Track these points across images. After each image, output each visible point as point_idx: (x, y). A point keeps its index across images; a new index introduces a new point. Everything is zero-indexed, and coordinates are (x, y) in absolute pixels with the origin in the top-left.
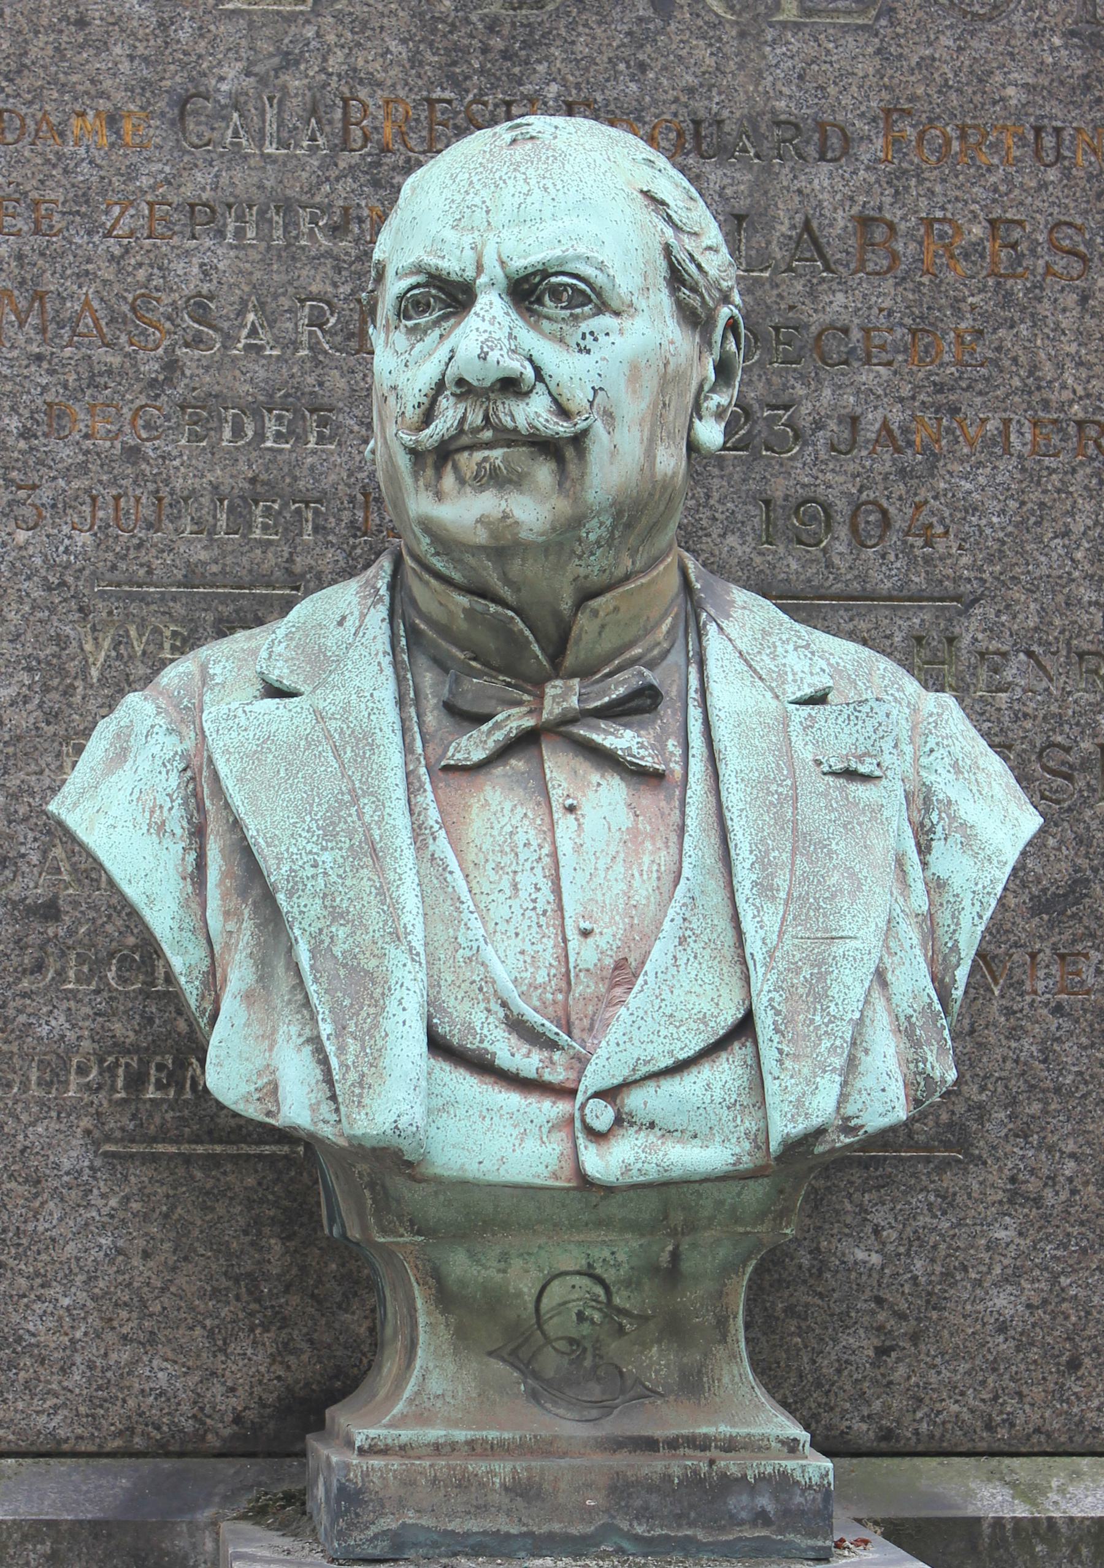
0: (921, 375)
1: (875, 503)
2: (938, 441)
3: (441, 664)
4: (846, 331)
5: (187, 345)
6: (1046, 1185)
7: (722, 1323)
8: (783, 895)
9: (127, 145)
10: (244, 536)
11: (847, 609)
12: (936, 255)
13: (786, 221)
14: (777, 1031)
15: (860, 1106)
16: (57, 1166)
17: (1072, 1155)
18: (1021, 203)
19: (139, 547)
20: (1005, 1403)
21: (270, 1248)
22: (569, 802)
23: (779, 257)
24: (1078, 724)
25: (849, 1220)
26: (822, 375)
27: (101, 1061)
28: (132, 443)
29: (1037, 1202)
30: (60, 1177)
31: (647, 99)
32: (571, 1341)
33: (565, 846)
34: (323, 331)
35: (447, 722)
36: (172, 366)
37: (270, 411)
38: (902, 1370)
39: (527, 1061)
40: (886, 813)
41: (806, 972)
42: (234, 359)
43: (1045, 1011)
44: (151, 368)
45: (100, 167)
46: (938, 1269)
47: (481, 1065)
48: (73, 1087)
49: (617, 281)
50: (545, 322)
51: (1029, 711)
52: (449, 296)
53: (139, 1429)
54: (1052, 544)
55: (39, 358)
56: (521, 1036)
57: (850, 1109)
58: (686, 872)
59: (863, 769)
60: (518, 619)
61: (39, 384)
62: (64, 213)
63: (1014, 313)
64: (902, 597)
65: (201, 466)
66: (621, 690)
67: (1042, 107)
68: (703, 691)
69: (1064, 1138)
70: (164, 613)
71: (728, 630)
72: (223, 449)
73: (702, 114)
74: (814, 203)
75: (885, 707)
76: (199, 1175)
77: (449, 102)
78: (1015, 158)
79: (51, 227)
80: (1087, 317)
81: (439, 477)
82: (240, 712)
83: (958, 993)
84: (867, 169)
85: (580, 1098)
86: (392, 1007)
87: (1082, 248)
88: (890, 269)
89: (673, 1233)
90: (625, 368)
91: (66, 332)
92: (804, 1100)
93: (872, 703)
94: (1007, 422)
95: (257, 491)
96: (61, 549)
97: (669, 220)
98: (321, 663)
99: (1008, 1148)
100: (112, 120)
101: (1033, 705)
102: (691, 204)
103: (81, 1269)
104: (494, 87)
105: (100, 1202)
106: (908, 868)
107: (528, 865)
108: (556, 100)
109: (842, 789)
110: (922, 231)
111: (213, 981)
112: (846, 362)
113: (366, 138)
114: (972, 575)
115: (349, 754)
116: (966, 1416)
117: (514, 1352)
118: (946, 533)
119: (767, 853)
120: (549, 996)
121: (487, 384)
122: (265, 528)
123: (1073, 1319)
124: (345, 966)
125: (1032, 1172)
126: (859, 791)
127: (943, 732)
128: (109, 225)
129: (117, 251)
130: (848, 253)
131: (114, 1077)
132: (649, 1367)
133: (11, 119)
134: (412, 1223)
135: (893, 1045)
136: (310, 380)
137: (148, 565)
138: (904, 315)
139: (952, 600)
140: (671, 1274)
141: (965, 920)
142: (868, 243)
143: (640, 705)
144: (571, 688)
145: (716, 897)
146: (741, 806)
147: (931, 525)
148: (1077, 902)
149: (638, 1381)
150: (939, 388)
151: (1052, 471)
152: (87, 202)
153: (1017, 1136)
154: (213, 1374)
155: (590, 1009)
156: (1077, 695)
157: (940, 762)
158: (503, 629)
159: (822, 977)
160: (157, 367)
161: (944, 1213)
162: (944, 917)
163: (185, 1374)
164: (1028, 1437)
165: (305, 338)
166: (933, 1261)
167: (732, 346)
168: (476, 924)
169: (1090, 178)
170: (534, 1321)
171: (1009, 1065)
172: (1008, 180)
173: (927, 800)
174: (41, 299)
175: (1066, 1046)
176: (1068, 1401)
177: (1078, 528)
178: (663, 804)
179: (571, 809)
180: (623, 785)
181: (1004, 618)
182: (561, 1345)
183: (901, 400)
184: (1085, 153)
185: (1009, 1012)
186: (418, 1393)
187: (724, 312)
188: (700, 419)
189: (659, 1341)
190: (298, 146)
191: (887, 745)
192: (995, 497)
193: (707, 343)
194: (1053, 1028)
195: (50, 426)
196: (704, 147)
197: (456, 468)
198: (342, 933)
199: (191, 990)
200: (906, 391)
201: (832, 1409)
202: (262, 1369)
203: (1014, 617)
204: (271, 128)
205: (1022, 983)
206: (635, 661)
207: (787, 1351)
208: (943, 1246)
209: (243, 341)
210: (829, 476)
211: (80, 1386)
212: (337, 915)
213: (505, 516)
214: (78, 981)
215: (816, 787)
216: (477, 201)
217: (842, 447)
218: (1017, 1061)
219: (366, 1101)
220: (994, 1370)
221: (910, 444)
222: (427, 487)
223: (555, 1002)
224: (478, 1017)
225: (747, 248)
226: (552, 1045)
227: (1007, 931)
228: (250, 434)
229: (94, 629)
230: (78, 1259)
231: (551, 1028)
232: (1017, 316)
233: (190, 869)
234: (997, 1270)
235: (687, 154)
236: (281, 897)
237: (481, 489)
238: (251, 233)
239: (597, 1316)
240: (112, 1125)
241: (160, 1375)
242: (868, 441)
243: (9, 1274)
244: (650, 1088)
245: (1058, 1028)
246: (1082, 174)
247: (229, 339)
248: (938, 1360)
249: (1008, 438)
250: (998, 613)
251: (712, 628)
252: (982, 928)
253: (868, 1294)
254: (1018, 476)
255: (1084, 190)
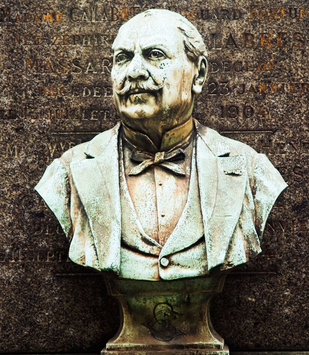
0: (261, 73)
1: (249, 106)
2: (266, 90)
3: (131, 149)
4: (241, 62)
5: (73, 71)
6: (298, 280)
7: (201, 315)
8: (213, 205)
9: (57, 22)
10: (89, 119)
11: (243, 134)
12: (264, 42)
13: (225, 35)
14: (210, 240)
15: (233, 259)
16: (44, 279)
17: (305, 273)
18: (286, 28)
19: (62, 123)
20: (288, 337)
21: (98, 300)
22: (160, 183)
23: (223, 44)
24: (303, 161)
25: (246, 290)
26: (235, 74)
27: (55, 252)
28: (60, 96)
29: (296, 285)
30: (45, 282)
31: (189, 5)
32: (163, 321)
33: (158, 194)
34: (108, 67)
35: (131, 164)
36: (70, 77)
37: (95, 87)
38: (261, 329)
39: (146, 248)
40: (242, 184)
41: (219, 224)
42: (86, 74)
43: (296, 236)
44: (64, 78)
45: (51, 27)
46: (270, 302)
47: (135, 250)
48: (48, 259)
49: (170, 50)
50: (152, 61)
51: (291, 158)
52: (128, 55)
53: (66, 346)
54: (296, 116)
55: (36, 76)
56: (145, 242)
57: (230, 260)
58: (189, 200)
59: (236, 173)
60: (148, 137)
61: (36, 82)
62: (42, 39)
63: (285, 57)
64: (258, 130)
65: (77, 102)
66: (175, 154)
67: (291, 3)
68: (196, 154)
69: (302, 268)
70: (69, 139)
71: (203, 139)
72: (83, 97)
73: (203, 8)
74: (232, 30)
75: (243, 157)
76: (80, 281)
77: (139, 8)
78: (284, 17)
79: (39, 43)
80: (304, 57)
81: (126, 101)
82: (79, 163)
83: (262, 230)
84: (246, 21)
85: (160, 258)
86: (112, 236)
87: (302, 39)
88: (252, 46)
89: (187, 293)
90: (173, 72)
91: (43, 69)
92: (216, 258)
93: (239, 156)
94: (283, 85)
95: (92, 108)
96: (43, 124)
97: (185, 34)
98: (101, 150)
99: (288, 271)
100: (54, 15)
101: (291, 157)
102: (192, 30)
103: (51, 305)
104: (150, 3)
105: (55, 288)
106: (249, 198)
107: (149, 199)
108: (166, 6)
109: (231, 178)
110: (261, 36)
111: (71, 231)
112: (241, 71)
113: (118, 18)
114: (275, 124)
115: (105, 172)
116: (278, 340)
117: (148, 324)
118: (268, 113)
119: (209, 195)
120: (154, 232)
121: (136, 77)
122: (94, 117)
123: (306, 315)
124: (101, 225)
125: (294, 277)
126: (234, 178)
127: (260, 163)
128: (53, 42)
129: (55, 48)
130: (241, 43)
131: (59, 256)
132: (183, 327)
133: (28, 16)
134: (121, 291)
135: (243, 243)
136: (105, 79)
137: (65, 127)
138: (256, 58)
139: (270, 130)
140: (188, 303)
141: (264, 211)
142: (247, 40)
143: (180, 158)
144: (162, 154)
145: (196, 206)
146: (203, 183)
147: (264, 112)
148: (304, 207)
149: (180, 331)
150: (266, 76)
151: (295, 97)
152: (48, 36)
153: (290, 268)
154: (85, 332)
155: (164, 236)
156: (303, 154)
157: (259, 171)
158: (144, 139)
159: (222, 226)
160: (66, 77)
161: (271, 288)
162: (259, 210)
163: (77, 332)
164: (295, 346)
165: (103, 69)
166: (269, 300)
167: (203, 66)
168: (135, 215)
169: (304, 21)
170: (153, 316)
171: (287, 249)
172: (283, 22)
173: (255, 181)
174: (37, 61)
175: (302, 244)
176: (305, 336)
177: (302, 111)
178: (184, 183)
179: (161, 185)
180: (174, 178)
181: (283, 135)
182: (160, 322)
183: (256, 80)
184: (303, 14)
185: (287, 236)
186: (123, 335)
187: (201, 58)
188: (195, 85)
189: (185, 321)
190: (100, 20)
191: (243, 167)
192: (280, 104)
193: (196, 66)
194: (299, 240)
195: (39, 93)
196: (204, 17)
197: (130, 99)
198: (100, 217)
199: (66, 232)
200: (257, 77)
201: (243, 339)
202: (97, 330)
203: (286, 134)
204: (94, 16)
205: (290, 228)
206: (180, 147)
207: (231, 324)
208: (271, 296)
209: (88, 70)
210: (238, 100)
211: (51, 335)
212: (99, 213)
213: (142, 111)
214: (49, 232)
215: (223, 177)
216: (135, 31)
217: (241, 92)
218: (289, 248)
219: (105, 260)
220: (285, 328)
221: (258, 91)
222: (123, 104)
223: (155, 234)
224: (135, 238)
225: (216, 42)
226: (153, 244)
227: (286, 215)
228: (90, 93)
229: (51, 144)
230: (50, 303)
231: (153, 240)
232: (286, 57)
233: (67, 202)
234: (286, 303)
235: (199, 19)
236: (85, 209)
237: (136, 104)
238: (89, 43)
239: (169, 314)
240: (58, 269)
241: (71, 332)
242: (247, 91)
243: (32, 307)
244: (178, 255)
245: (300, 240)
246: (302, 20)
247: (84, 70)
248: (271, 326)
249: (284, 89)
250: (282, 134)
251: (199, 138)
252: (269, 213)
253: (252, 309)
254: (287, 98)
255: (302, 24)
